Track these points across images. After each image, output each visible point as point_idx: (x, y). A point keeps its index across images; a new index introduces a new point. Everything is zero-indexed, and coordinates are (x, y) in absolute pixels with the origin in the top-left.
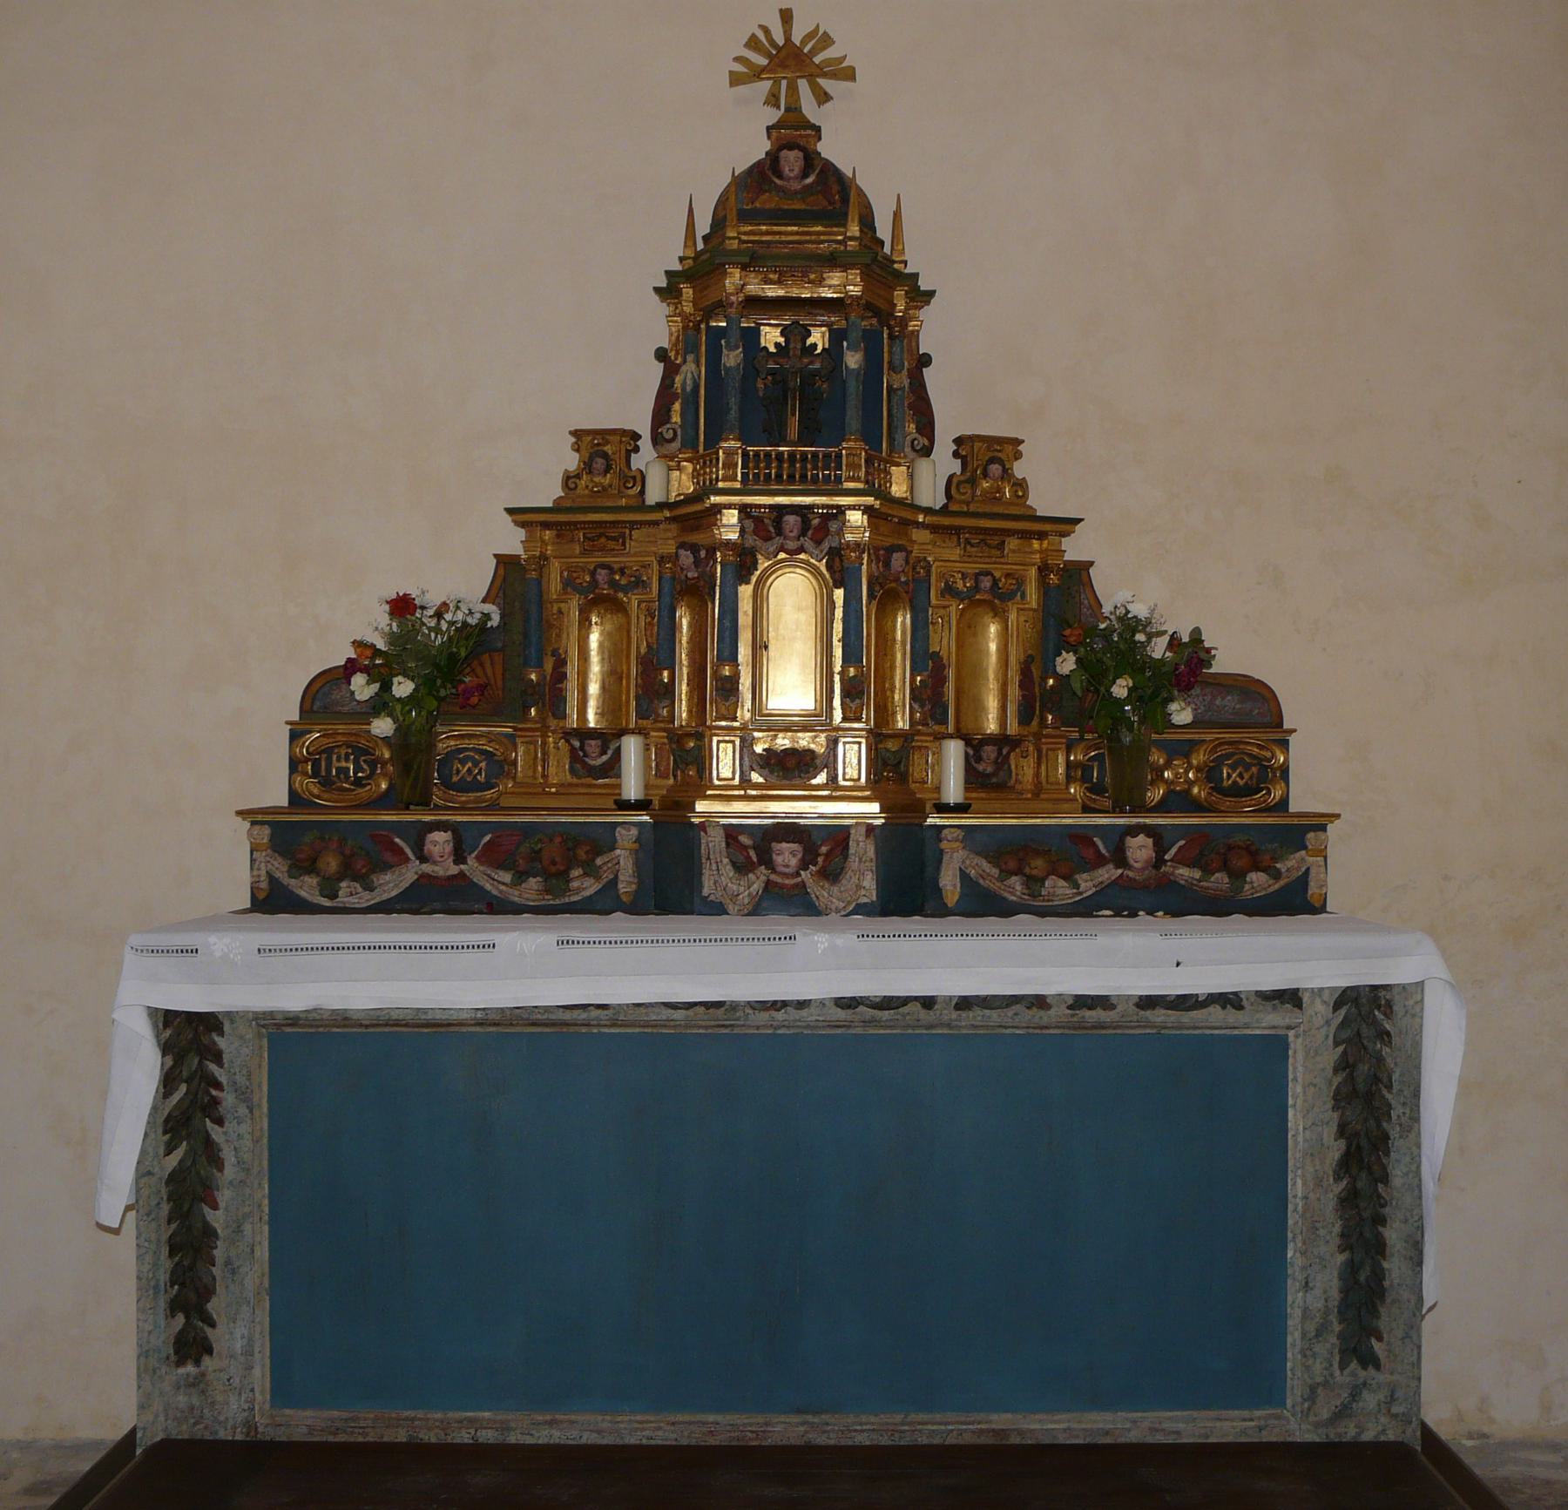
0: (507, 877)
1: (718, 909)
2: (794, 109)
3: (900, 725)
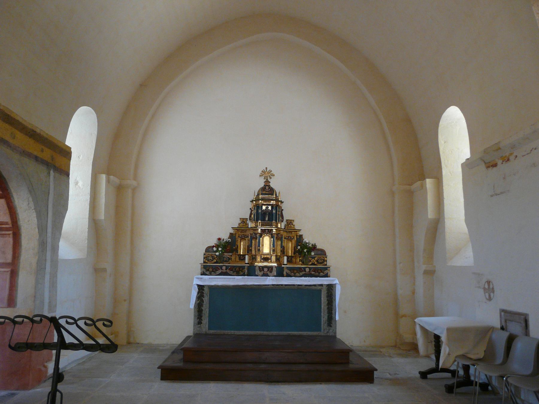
0: (232, 272)
2: (267, 180)
3: (279, 254)
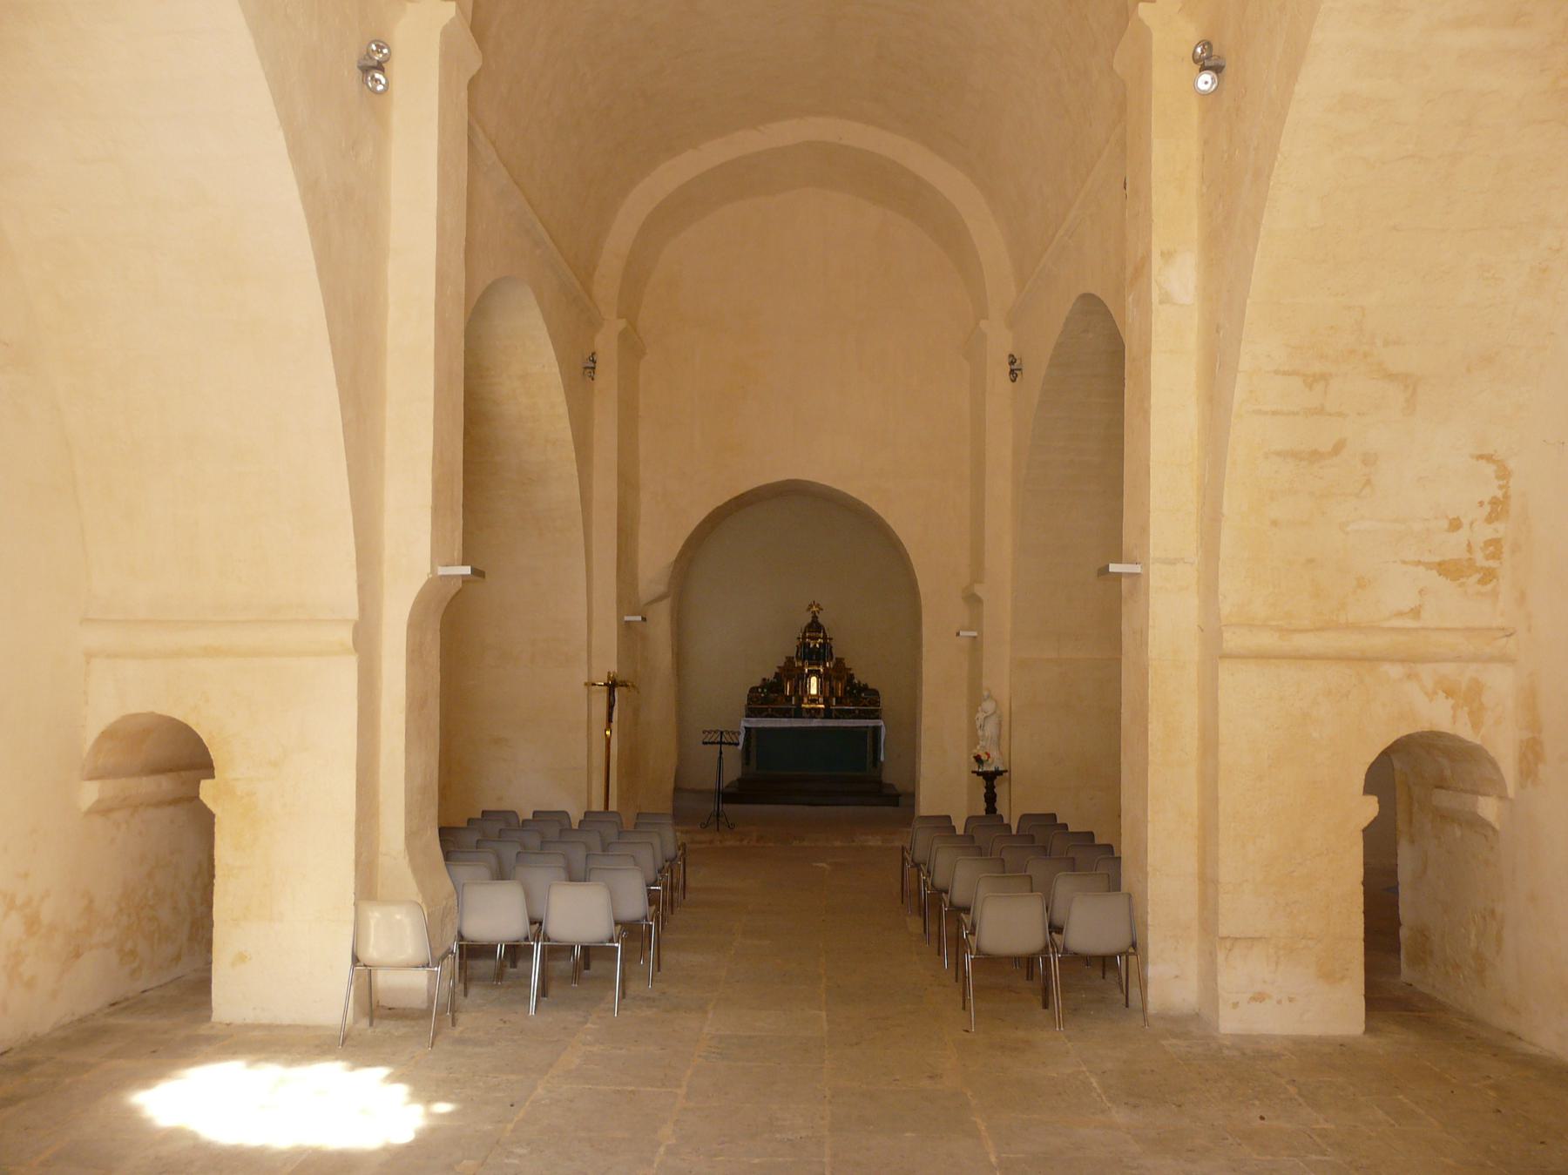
1: (804, 718)
